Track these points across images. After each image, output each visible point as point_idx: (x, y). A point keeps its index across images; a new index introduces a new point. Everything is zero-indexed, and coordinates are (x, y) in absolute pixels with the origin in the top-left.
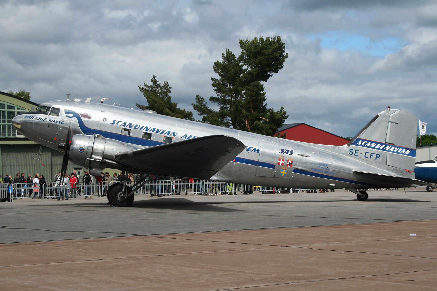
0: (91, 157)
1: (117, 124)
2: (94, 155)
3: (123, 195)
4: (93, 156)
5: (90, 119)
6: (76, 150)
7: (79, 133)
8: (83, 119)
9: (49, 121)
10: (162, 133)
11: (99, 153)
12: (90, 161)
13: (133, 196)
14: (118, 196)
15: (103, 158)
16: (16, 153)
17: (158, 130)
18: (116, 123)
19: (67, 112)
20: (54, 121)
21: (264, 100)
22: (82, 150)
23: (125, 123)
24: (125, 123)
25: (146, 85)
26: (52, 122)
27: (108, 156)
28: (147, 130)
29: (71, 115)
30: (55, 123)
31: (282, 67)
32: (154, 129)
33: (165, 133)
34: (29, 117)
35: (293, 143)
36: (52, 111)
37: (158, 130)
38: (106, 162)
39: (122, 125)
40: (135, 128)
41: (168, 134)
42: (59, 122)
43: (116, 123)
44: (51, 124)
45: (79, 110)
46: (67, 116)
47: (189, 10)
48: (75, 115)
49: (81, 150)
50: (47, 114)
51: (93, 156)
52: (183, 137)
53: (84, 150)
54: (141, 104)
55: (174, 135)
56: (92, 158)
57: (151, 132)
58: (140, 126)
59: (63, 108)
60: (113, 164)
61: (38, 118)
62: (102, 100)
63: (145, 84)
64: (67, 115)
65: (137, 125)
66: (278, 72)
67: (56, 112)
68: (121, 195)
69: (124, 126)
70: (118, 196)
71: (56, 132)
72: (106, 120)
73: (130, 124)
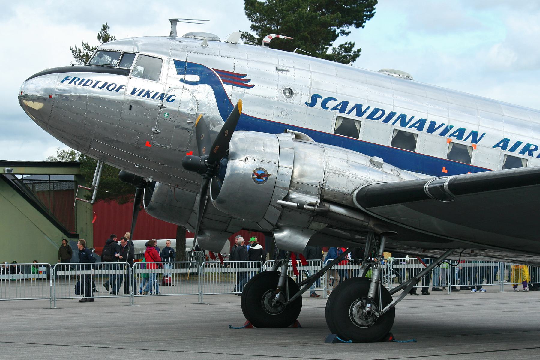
0: (286, 199)
1: (324, 105)
2: (297, 190)
5: (247, 90)
6: (245, 175)
8: (228, 88)
9: (133, 92)
10: (443, 134)
12: (284, 206)
13: (299, 301)
14: (354, 311)
15: (323, 200)
16: (394, 184)
17: (433, 123)
18: (319, 101)
20: (148, 94)
23: (345, 104)
24: (345, 104)
25: (87, 47)
26: (141, 98)
27: (336, 194)
28: (403, 124)
29: (196, 78)
31: (372, 15)
32: (422, 122)
33: (453, 135)
37: (433, 123)
38: (329, 211)
39: (335, 108)
40: (371, 117)
42: (162, 97)
44: (137, 102)
46: (182, 81)
49: (259, 177)
50: (126, 73)
51: (293, 195)
52: (497, 145)
53: (267, 176)
56: (291, 200)
57: (414, 130)
58: (384, 112)
61: (100, 85)
63: (83, 45)
64: (182, 76)
68: (363, 307)
69: (342, 110)
70: (354, 311)
72: (291, 92)
73: (358, 107)
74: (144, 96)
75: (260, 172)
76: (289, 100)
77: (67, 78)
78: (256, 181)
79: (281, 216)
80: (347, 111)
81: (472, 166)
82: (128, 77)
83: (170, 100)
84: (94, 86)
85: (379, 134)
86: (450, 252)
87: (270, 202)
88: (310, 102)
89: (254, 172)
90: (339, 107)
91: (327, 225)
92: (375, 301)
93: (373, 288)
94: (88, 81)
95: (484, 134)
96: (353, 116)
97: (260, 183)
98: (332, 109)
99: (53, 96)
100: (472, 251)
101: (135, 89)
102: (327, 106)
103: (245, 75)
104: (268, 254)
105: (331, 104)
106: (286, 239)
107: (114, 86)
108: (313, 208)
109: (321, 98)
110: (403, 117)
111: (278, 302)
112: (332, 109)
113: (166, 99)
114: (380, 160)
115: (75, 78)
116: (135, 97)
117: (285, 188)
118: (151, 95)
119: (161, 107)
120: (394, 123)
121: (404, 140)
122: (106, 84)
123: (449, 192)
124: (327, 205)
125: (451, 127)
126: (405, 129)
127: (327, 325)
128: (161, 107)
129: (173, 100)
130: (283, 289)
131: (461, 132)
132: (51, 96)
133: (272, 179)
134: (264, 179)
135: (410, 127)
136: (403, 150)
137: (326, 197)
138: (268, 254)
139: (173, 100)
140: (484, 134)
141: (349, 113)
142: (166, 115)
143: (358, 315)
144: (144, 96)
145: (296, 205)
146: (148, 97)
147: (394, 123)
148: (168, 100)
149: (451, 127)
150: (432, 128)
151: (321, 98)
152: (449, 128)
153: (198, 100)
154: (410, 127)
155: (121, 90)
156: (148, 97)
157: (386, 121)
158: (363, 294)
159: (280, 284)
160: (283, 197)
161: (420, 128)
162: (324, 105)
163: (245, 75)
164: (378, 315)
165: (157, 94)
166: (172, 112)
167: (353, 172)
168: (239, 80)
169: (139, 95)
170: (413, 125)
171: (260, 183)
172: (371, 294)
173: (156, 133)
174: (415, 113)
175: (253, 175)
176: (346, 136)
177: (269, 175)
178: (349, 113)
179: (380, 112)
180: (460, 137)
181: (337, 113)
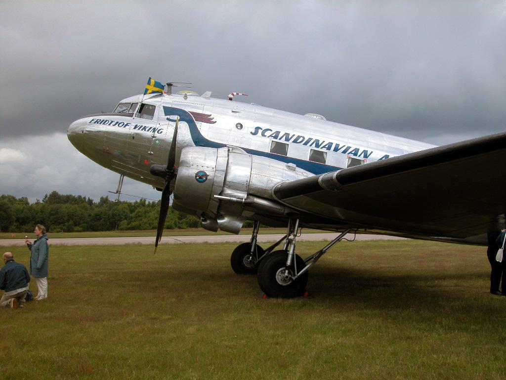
2: (230, 187)
3: (289, 273)
4: (228, 191)
7: (191, 146)
9: (135, 128)
10: (344, 152)
12: (220, 200)
15: (249, 194)
17: (337, 145)
18: (260, 131)
20: (145, 128)
21: (85, 198)
22: (202, 177)
24: (278, 133)
26: (140, 132)
28: (317, 146)
29: (176, 117)
32: (330, 145)
33: (351, 153)
34: (97, 122)
36: (140, 111)
37: (337, 145)
39: (271, 136)
40: (295, 141)
41: (355, 154)
44: (137, 134)
46: (168, 119)
50: (131, 115)
53: (206, 176)
55: (366, 156)
57: (324, 150)
60: (262, 205)
61: (113, 124)
62: (230, 96)
64: (168, 117)
65: (299, 137)
66: (102, 198)
69: (276, 137)
71: (149, 150)
72: (242, 126)
75: (201, 174)
76: (239, 131)
78: (197, 179)
80: (279, 138)
81: (326, 165)
83: (159, 132)
85: (304, 154)
86: (348, 231)
87: (210, 197)
91: (254, 213)
92: (291, 268)
93: (290, 257)
94: (106, 121)
95: (372, 152)
96: (283, 141)
98: (269, 137)
99: (84, 132)
100: (365, 230)
101: (136, 125)
102: (265, 134)
103: (211, 115)
105: (268, 133)
106: (225, 224)
109: (262, 129)
110: (317, 142)
111: (250, 261)
112: (269, 137)
113: (156, 132)
114: (294, 166)
115: (98, 120)
116: (136, 131)
117: (220, 186)
118: (147, 129)
119: (154, 137)
120: (311, 145)
121: (317, 156)
122: (117, 122)
123: (338, 183)
124: (251, 197)
125: (349, 148)
126: (319, 149)
128: (154, 137)
129: (161, 132)
130: (254, 252)
131: (356, 152)
132: (83, 132)
133: (210, 179)
135: (322, 148)
136: (316, 163)
137: (253, 192)
139: (161, 132)
140: (372, 152)
141: (280, 139)
143: (280, 277)
144: (142, 130)
146: (145, 130)
147: (311, 145)
148: (158, 132)
149: (349, 148)
150: (336, 150)
151: (262, 129)
152: (349, 148)
154: (322, 148)
155: (127, 127)
156: (145, 130)
157: (306, 144)
158: (283, 263)
159: (252, 250)
161: (329, 148)
162: (263, 135)
163: (211, 115)
164: (294, 278)
166: (159, 140)
167: (278, 175)
168: (207, 119)
169: (139, 129)
170: (324, 147)
172: (289, 262)
173: (150, 154)
174: (324, 139)
175: (196, 177)
176: (279, 153)
177: (208, 175)
179: (301, 139)
180: (355, 154)
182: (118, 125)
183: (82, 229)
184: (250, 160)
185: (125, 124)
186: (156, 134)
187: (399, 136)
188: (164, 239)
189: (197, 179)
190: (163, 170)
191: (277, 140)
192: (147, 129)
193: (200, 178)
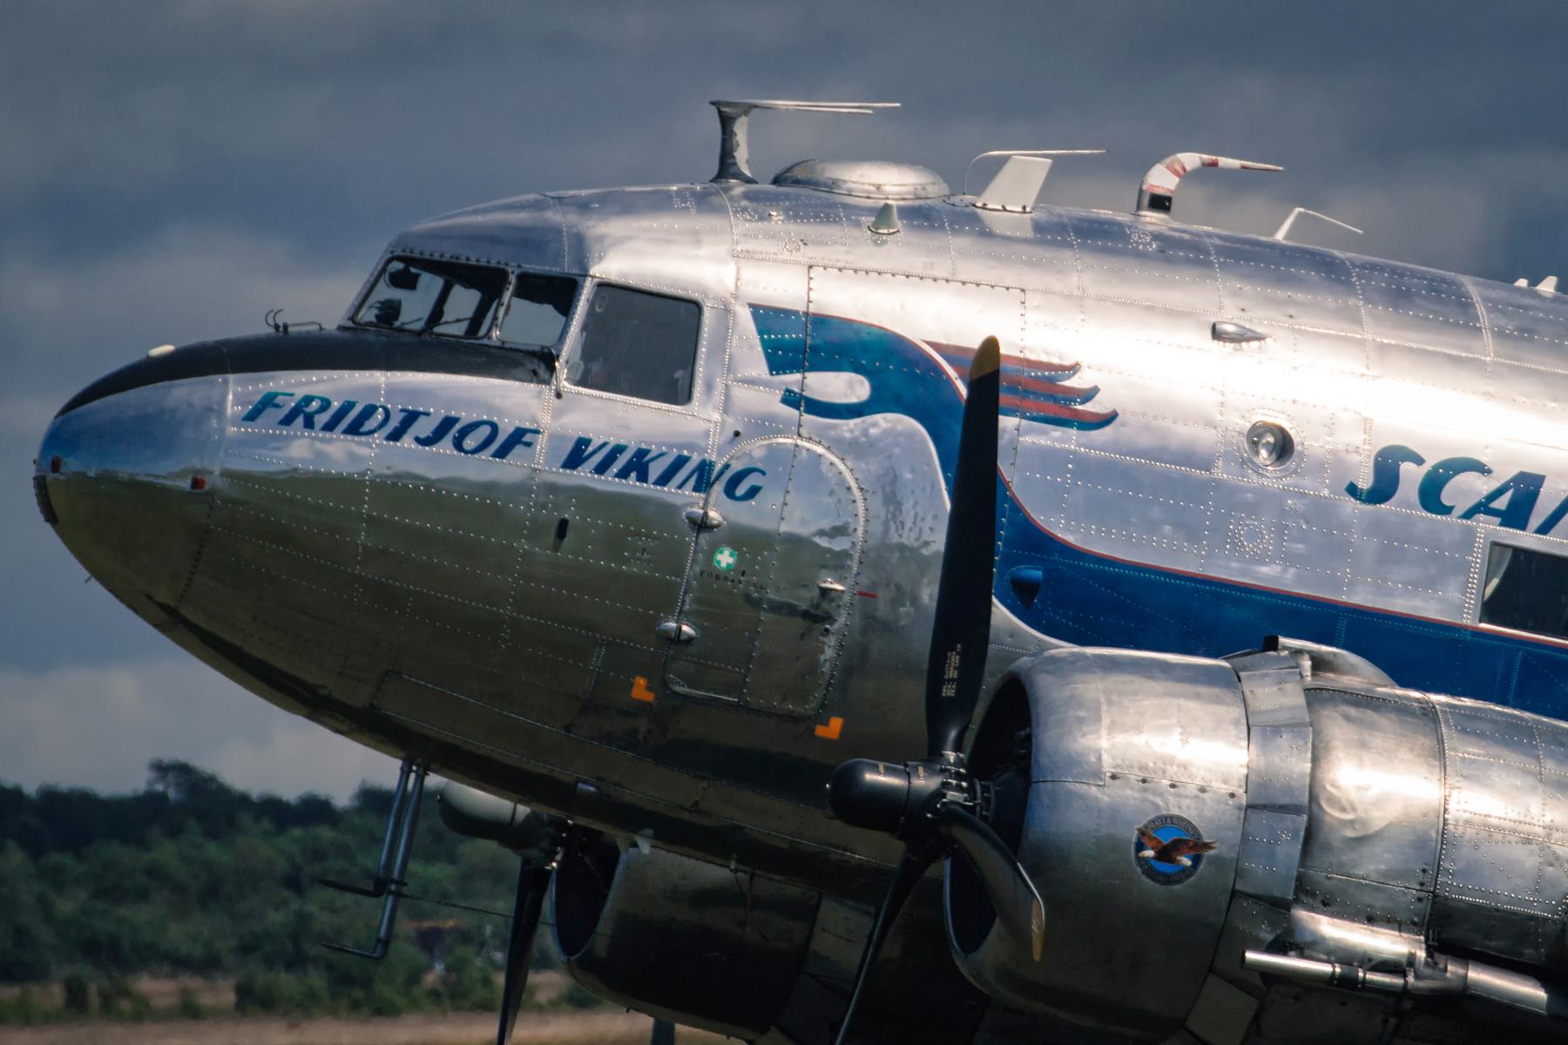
1: (1431, 495)
11: (1371, 865)
19: (800, 343)
22: (1173, 843)
26: (609, 483)
29: (844, 386)
30: (648, 489)
35: (1166, 668)
39: (1483, 507)
43: (1411, 475)
44: (587, 497)
45: (938, 306)
46: (791, 399)
47: (160, 787)
48: (896, 370)
49: (1165, 853)
53: (1197, 847)
54: (1255, 344)
59: (723, 265)
61: (423, 427)
64: (792, 379)
67: (653, 341)
69: (1516, 515)
74: (624, 474)
77: (268, 402)
78: (1151, 873)
79: (1257, 1018)
80: (1536, 520)
82: (548, 392)
83: (741, 490)
84: (395, 436)
88: (1365, 482)
89: (1142, 833)
90: (1501, 503)
97: (1168, 880)
98: (1468, 515)
102: (1446, 498)
103: (1074, 369)
104: (1037, 957)
107: (485, 431)
108: (1397, 981)
112: (1468, 515)
113: (718, 488)
115: (308, 400)
118: (655, 470)
122: (448, 423)
127: (925, 666)
129: (753, 492)
133: (1218, 861)
134: (1186, 861)
138: (1037, 957)
142: (725, 559)
144: (624, 474)
145: (1326, 968)
148: (730, 490)
151: (1419, 461)
153: (871, 492)
156: (643, 477)
160: (1269, 937)
163: (1074, 369)
165: (680, 462)
169: (601, 469)
171: (1168, 880)
175: (1140, 847)
177: (1207, 846)
178: (1544, 529)
181: (1488, 528)
182: (458, 445)
183: (83, 894)
184: (1237, 712)
185: (448, 440)
186: (1364, 370)
187: (236, 681)
188: (522, 1030)
189: (1142, 861)
190: (435, 772)
191: (1527, 539)
192: (655, 470)
193: (1165, 853)
